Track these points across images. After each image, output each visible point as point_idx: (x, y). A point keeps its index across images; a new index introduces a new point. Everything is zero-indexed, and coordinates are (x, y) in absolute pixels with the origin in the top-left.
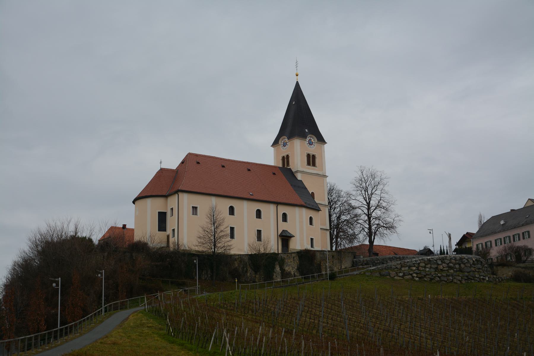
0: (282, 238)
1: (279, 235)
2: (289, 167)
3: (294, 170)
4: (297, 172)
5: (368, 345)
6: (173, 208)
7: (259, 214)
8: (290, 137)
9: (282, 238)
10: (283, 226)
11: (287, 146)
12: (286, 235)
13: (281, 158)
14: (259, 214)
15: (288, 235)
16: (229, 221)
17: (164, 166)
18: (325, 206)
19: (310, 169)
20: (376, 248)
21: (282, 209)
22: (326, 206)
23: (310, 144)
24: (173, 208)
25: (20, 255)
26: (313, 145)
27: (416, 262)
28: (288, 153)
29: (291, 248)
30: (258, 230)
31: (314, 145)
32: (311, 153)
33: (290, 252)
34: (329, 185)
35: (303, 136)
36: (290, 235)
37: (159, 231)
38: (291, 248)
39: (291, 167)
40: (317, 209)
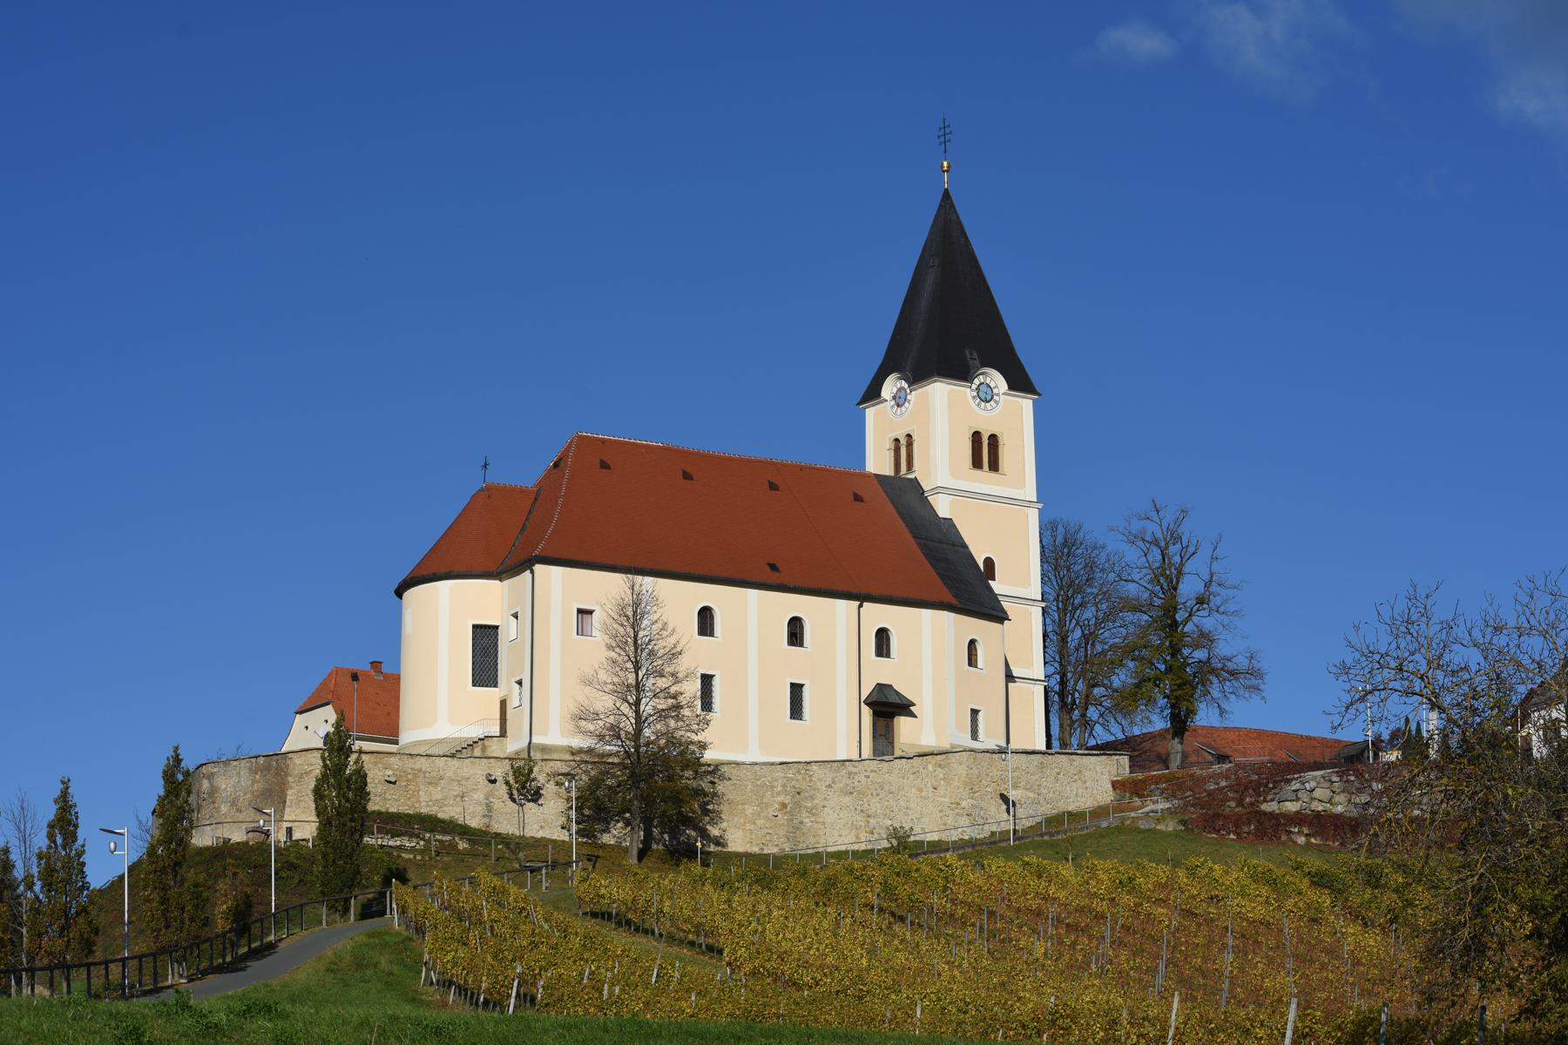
0: (876, 708)
1: (863, 700)
2: (911, 476)
3: (322, 741)
4: (937, 490)
5: (1040, 1016)
6: (517, 612)
7: (795, 631)
8: (918, 376)
9: (876, 708)
10: (879, 672)
11: (906, 404)
12: (885, 700)
13: (889, 445)
14: (795, 631)
15: (894, 699)
16: (698, 655)
17: (499, 477)
18: (1031, 603)
19: (983, 482)
20: (1223, 739)
21: (878, 615)
22: (1036, 603)
23: (987, 401)
24: (517, 612)
25: (585, 732)
26: (992, 402)
27: (1302, 787)
28: (910, 428)
29: (902, 741)
30: (793, 685)
31: (997, 403)
32: (985, 474)
33: (898, 753)
34: (1061, 530)
35: (961, 373)
36: (899, 701)
37: (474, 685)
38: (902, 741)
39: (918, 473)
40: (1000, 616)
